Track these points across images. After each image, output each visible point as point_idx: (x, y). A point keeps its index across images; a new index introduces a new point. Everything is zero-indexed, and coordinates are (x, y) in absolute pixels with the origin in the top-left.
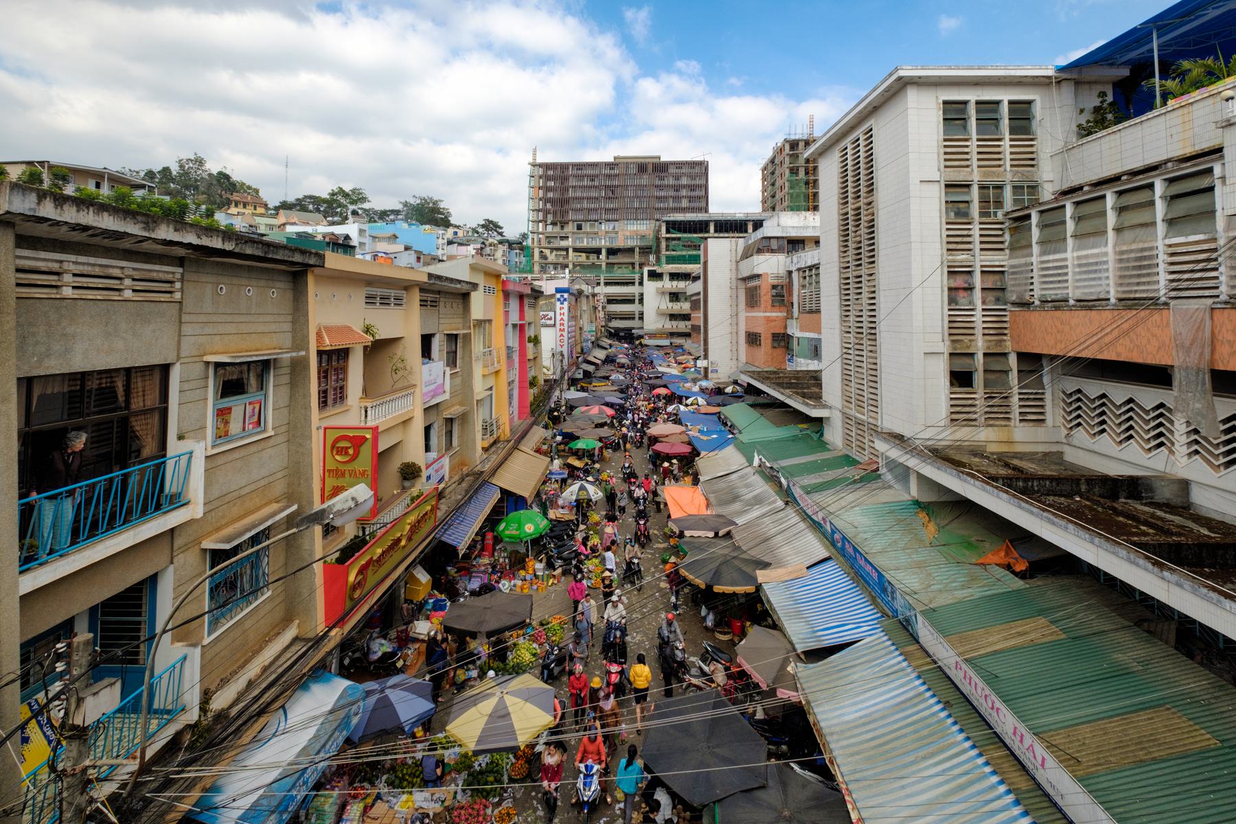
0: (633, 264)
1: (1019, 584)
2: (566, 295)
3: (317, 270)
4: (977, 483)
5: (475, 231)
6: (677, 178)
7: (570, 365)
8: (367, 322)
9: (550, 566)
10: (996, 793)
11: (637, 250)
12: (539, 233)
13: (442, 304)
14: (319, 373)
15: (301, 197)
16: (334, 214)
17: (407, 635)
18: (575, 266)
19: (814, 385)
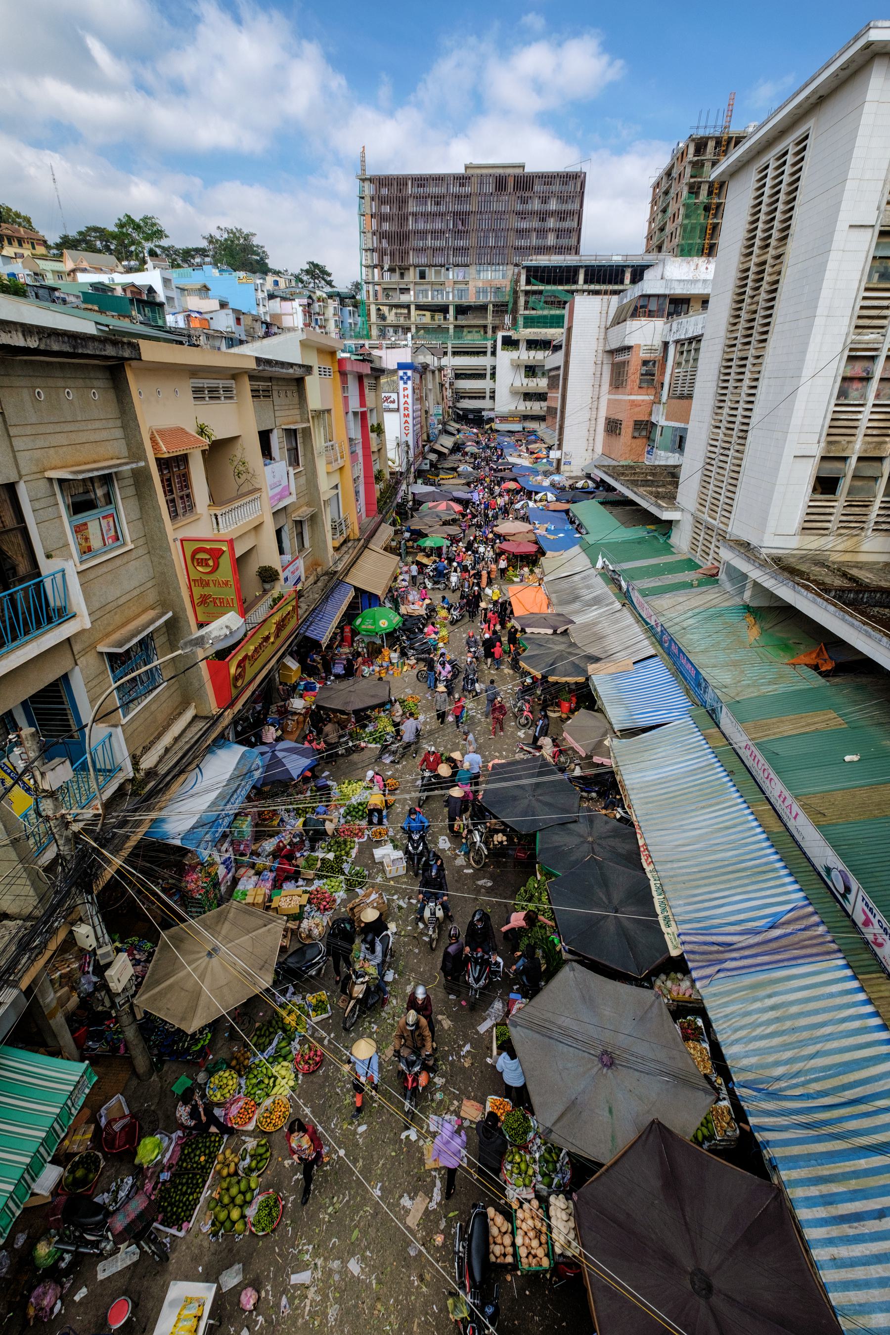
0: (485, 327)
1: (821, 681)
2: (409, 373)
3: (134, 363)
4: (810, 595)
5: (299, 279)
6: (545, 200)
7: (416, 457)
8: (200, 422)
9: (403, 654)
10: (753, 832)
11: (490, 307)
12: (375, 284)
13: (275, 394)
14: (162, 481)
15: (83, 229)
16: (129, 256)
17: (286, 709)
18: (418, 329)
19: (670, 483)
